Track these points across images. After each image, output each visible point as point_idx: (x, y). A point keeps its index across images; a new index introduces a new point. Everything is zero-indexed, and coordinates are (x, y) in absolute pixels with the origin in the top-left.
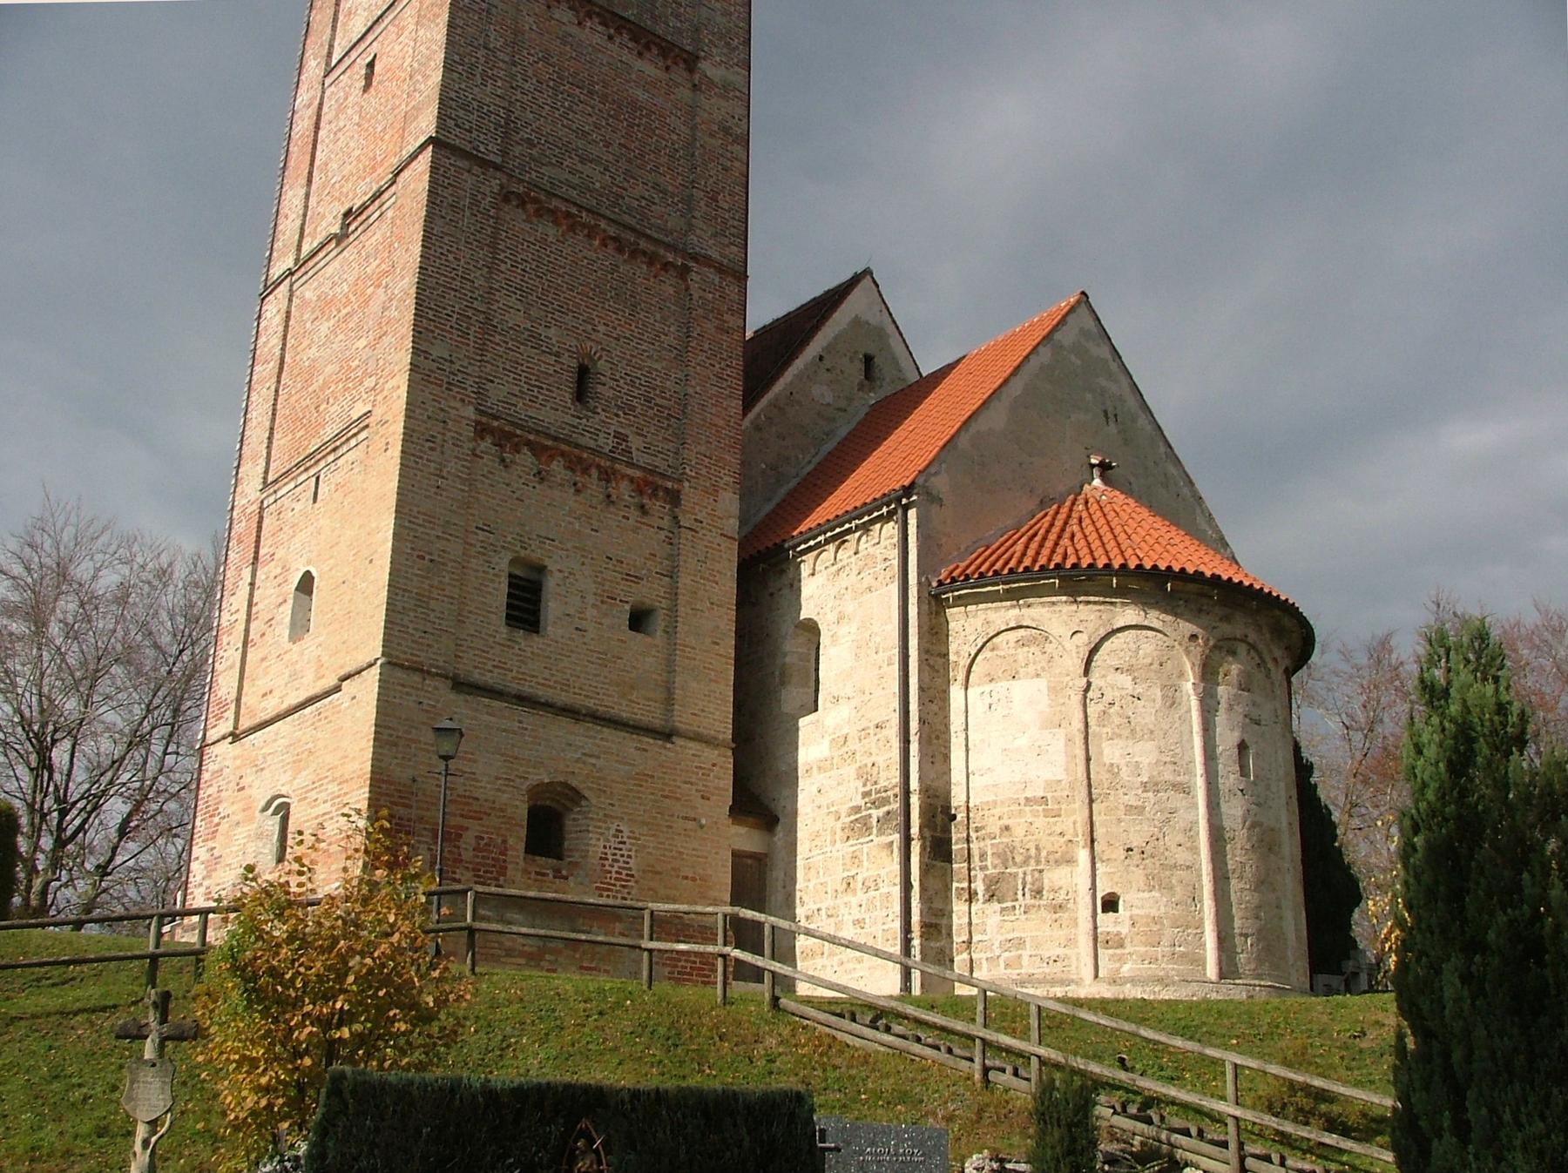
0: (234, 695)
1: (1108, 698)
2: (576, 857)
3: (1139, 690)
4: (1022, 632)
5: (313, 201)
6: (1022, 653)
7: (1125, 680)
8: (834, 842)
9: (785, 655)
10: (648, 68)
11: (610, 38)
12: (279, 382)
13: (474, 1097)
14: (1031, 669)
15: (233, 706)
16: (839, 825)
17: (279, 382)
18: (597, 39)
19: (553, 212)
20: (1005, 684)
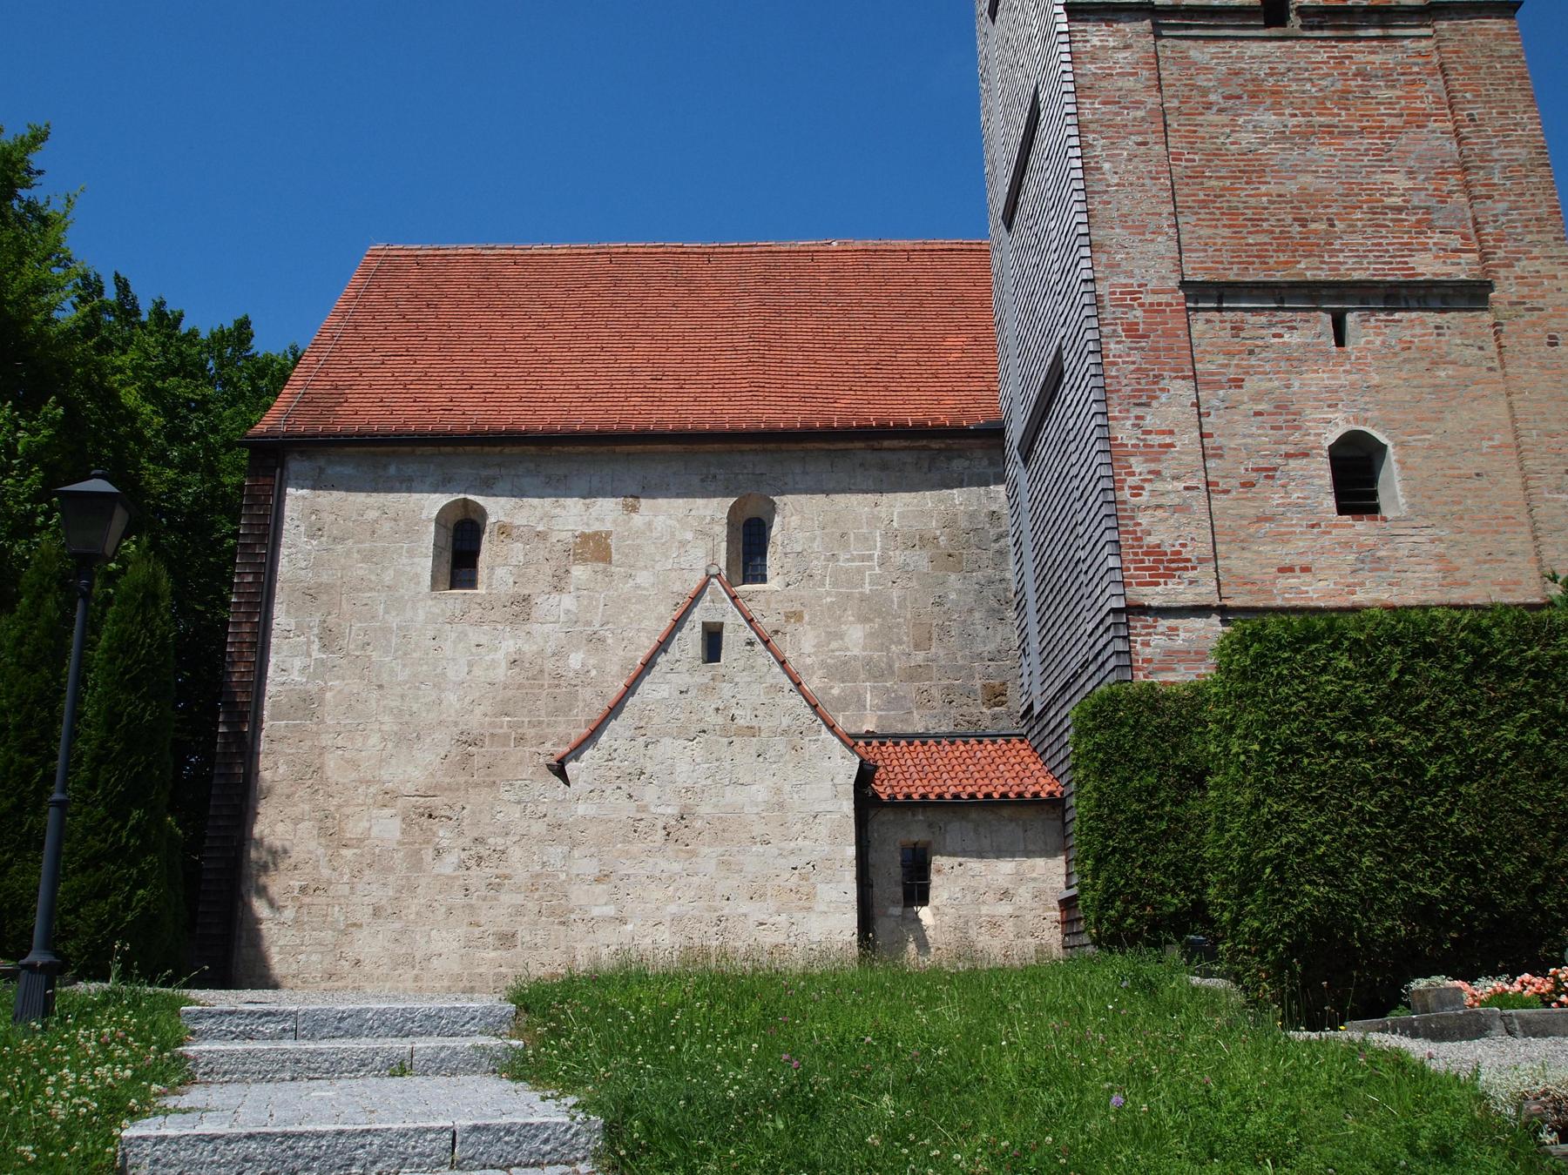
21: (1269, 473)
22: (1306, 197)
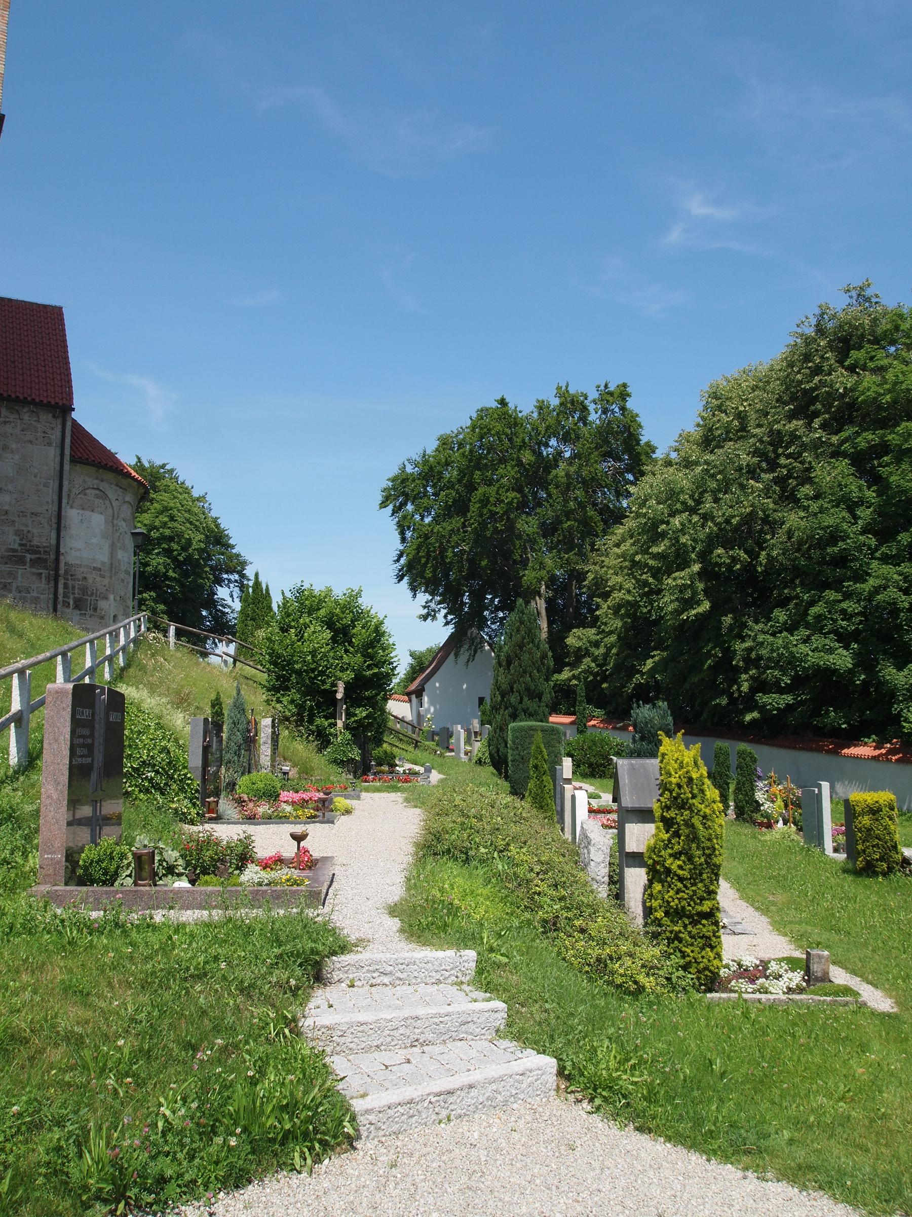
4: (97, 492)
6: (97, 501)
20: (90, 513)
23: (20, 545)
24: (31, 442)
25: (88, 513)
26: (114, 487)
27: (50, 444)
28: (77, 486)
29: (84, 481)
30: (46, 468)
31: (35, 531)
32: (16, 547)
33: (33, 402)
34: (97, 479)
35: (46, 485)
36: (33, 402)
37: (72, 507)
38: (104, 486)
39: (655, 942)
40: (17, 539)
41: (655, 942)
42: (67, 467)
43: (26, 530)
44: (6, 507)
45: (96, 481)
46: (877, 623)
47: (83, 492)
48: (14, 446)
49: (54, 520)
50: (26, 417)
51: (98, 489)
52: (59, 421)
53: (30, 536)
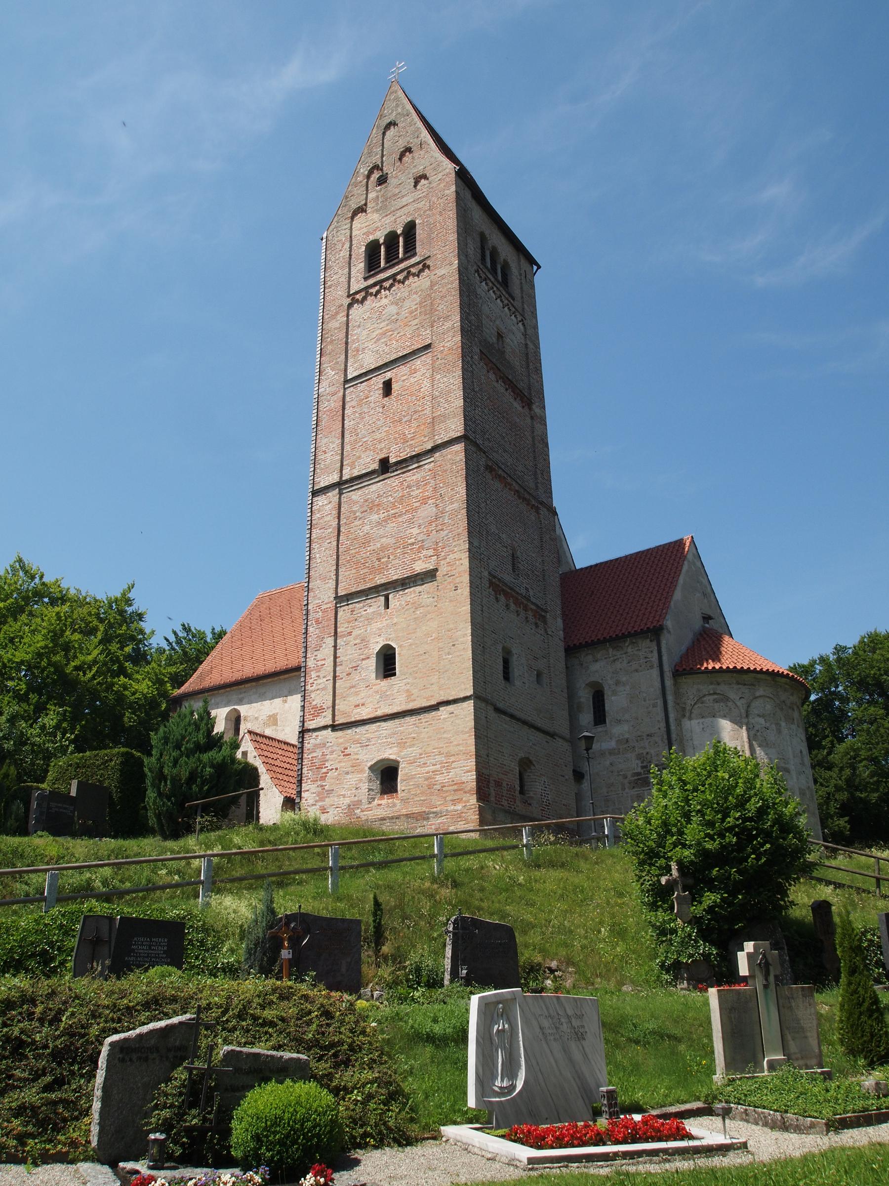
0: (330, 703)
1: (756, 728)
2: (531, 794)
3: (768, 725)
4: (716, 696)
5: (347, 448)
6: (716, 705)
7: (762, 721)
8: (623, 789)
9: (580, 697)
10: (517, 405)
11: (507, 390)
12: (338, 541)
13: (788, 879)
14: (722, 713)
15: (330, 710)
16: (626, 781)
17: (338, 541)
18: (503, 390)
19: (500, 476)
20: (711, 719)
21: (355, 668)
22: (383, 548)
23: (643, 767)
24: (637, 671)
25: (708, 720)
26: (736, 687)
27: (652, 667)
28: (691, 697)
29: (699, 690)
30: (652, 690)
31: (652, 751)
32: (639, 770)
33: (630, 635)
34: (712, 684)
35: (655, 706)
36: (630, 635)
37: (690, 719)
38: (722, 688)
39: (140, 637)
40: (639, 762)
41: (140, 637)
42: (669, 682)
43: (645, 752)
44: (627, 736)
45: (711, 687)
46: (64, 735)
47: (700, 700)
48: (624, 679)
49: (665, 737)
50: (611, 650)
51: (715, 693)
52: (654, 643)
53: (649, 757)
